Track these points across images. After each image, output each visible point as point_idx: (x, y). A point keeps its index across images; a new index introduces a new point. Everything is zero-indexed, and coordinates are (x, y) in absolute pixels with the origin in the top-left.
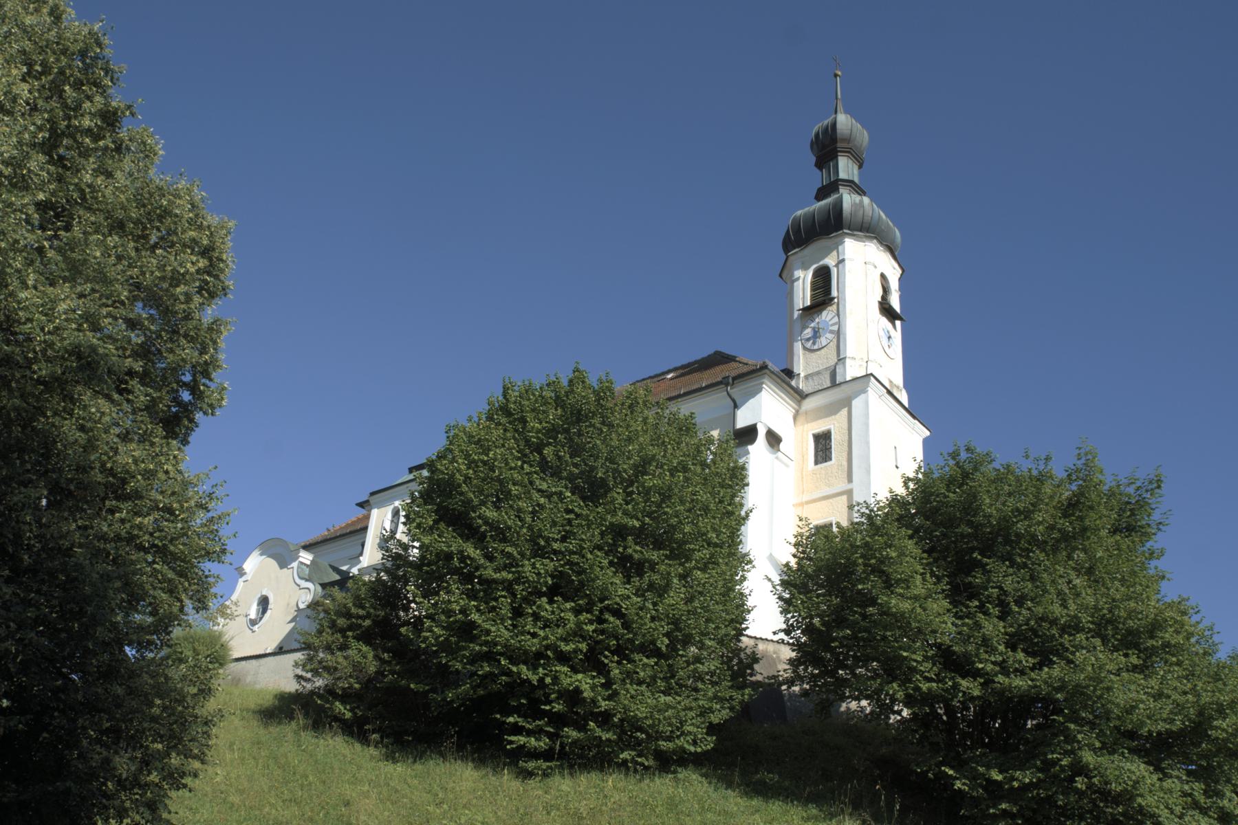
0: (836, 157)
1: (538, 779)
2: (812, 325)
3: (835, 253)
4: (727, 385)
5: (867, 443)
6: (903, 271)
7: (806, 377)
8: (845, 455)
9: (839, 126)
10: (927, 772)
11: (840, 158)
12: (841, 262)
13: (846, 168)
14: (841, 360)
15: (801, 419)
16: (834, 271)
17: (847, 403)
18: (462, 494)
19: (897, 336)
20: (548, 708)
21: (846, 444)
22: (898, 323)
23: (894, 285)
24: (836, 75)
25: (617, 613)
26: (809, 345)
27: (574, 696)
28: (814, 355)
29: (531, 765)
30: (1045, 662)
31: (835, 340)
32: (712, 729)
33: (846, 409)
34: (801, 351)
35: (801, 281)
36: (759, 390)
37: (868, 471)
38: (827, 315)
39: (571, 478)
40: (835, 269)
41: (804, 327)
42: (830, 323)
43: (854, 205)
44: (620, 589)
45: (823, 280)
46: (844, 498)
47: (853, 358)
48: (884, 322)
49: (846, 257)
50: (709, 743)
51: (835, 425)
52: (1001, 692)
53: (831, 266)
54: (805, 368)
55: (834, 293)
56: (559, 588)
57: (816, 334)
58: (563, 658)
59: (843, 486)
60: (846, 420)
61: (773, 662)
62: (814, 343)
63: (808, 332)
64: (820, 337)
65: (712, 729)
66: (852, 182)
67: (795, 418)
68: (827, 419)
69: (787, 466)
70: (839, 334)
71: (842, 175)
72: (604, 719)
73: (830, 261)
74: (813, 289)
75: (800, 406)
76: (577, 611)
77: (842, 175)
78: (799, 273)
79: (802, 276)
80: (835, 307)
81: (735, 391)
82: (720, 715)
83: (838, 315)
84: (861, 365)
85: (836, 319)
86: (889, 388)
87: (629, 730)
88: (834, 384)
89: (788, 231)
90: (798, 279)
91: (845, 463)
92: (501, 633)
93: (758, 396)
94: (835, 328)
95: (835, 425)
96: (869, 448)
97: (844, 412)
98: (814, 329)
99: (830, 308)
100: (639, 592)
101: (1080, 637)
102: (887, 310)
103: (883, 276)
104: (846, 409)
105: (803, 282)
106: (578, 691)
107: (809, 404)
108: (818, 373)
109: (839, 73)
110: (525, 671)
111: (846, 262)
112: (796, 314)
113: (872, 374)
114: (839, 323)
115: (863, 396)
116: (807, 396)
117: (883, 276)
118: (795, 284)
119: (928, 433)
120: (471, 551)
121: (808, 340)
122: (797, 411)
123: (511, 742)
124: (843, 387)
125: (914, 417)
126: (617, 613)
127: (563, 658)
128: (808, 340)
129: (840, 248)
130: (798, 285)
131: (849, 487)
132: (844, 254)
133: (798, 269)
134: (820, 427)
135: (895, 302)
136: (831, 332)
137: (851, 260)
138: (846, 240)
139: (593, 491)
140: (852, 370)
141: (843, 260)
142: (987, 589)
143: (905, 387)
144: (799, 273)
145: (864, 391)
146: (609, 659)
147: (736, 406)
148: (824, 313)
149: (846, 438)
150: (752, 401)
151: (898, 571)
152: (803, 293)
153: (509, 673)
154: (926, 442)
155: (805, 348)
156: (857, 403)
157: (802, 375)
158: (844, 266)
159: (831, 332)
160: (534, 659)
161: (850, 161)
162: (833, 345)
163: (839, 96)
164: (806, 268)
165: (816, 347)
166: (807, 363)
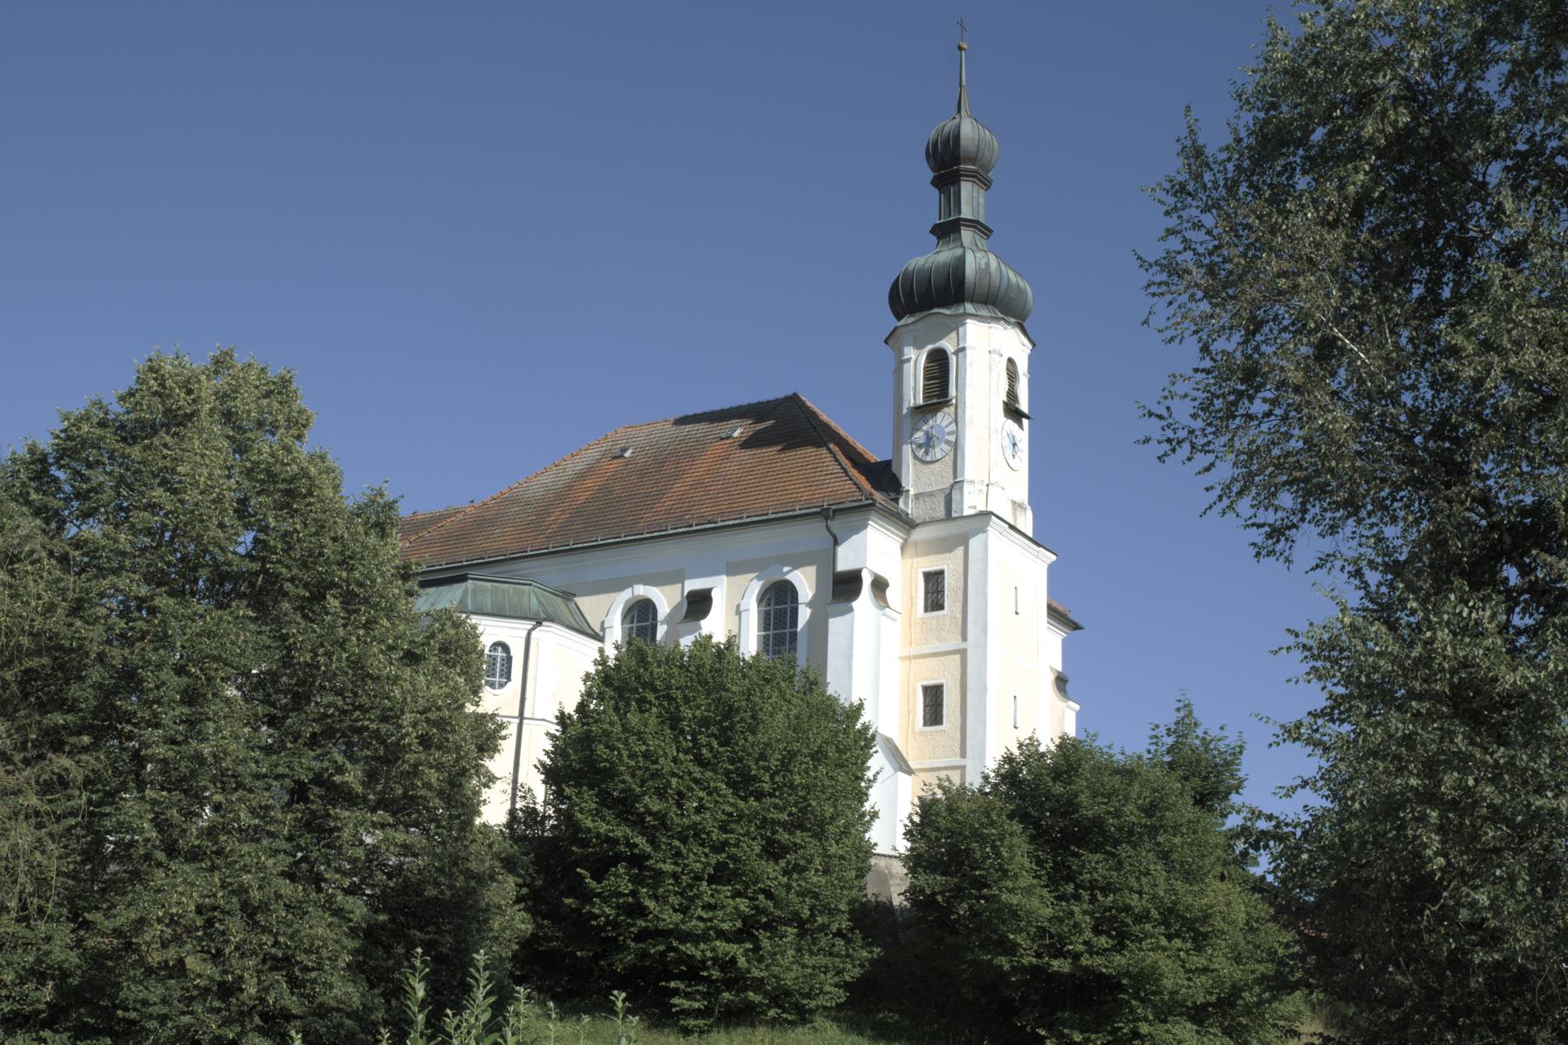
0: (958, 182)
1: (696, 1035)
2: (925, 428)
3: (954, 335)
4: (827, 518)
5: (985, 596)
6: (1034, 345)
7: (917, 496)
8: (959, 605)
9: (963, 141)
10: (1026, 1026)
11: (963, 184)
12: (961, 350)
13: (971, 199)
14: (957, 484)
15: (909, 550)
16: (953, 360)
17: (963, 540)
18: (624, 782)
19: (1022, 435)
20: (705, 974)
21: (961, 593)
22: (1025, 422)
23: (1022, 367)
24: (960, 49)
25: (769, 895)
26: (920, 453)
27: (728, 964)
28: (925, 468)
29: (692, 1022)
30: (1120, 947)
31: (952, 454)
32: (847, 986)
33: (962, 548)
34: (911, 460)
35: (912, 363)
36: (865, 526)
37: (984, 631)
38: (942, 419)
39: (727, 773)
40: (954, 358)
41: (915, 429)
42: (947, 430)
43: (979, 271)
44: (771, 872)
45: (939, 367)
46: (957, 657)
47: (972, 482)
48: (1011, 425)
49: (968, 344)
50: (842, 996)
51: (948, 563)
52: (1086, 969)
53: (949, 353)
54: (915, 484)
55: (952, 391)
56: (719, 876)
57: (929, 443)
58: (721, 934)
59: (956, 643)
60: (961, 561)
61: (884, 878)
62: (927, 453)
63: (919, 436)
64: (934, 447)
65: (847, 986)
66: (977, 222)
67: (903, 548)
68: (940, 556)
69: (894, 620)
70: (956, 447)
71: (966, 212)
72: (758, 985)
73: (948, 345)
74: (926, 379)
75: (909, 536)
76: (736, 894)
77: (966, 212)
78: (910, 352)
79: (914, 357)
80: (952, 409)
81: (836, 525)
82: (852, 973)
83: (956, 421)
84: (980, 491)
85: (953, 427)
86: (1012, 523)
87: (780, 997)
88: (949, 515)
89: (897, 280)
90: (909, 360)
91: (959, 616)
92: (670, 918)
93: (862, 533)
94: (952, 438)
95: (948, 563)
96: (986, 603)
97: (960, 551)
98: (927, 433)
99: (946, 410)
100: (786, 872)
101: (1148, 927)
102: (1012, 412)
103: (1010, 361)
104: (962, 548)
105: (916, 360)
106: (733, 960)
107: (919, 534)
108: (931, 494)
109: (965, 46)
110: (689, 949)
111: (968, 351)
112: (905, 411)
113: (992, 513)
114: (956, 432)
115: (981, 536)
116: (917, 525)
117: (1010, 361)
118: (906, 366)
119: (1054, 558)
120: (640, 840)
121: (920, 446)
122: (905, 540)
123: (675, 1006)
124: (960, 522)
125: (1038, 545)
126: (769, 895)
127: (721, 934)
128: (920, 446)
129: (961, 329)
130: (909, 368)
131: (963, 646)
132: (965, 341)
133: (909, 345)
134: (932, 563)
135: (1024, 406)
136: (948, 442)
137: (974, 348)
138: (969, 321)
139: (743, 783)
140: (971, 502)
141: (964, 349)
142: (1081, 874)
143: (1030, 503)
144: (910, 352)
145: (984, 531)
146: (762, 935)
147: (836, 543)
148: (940, 415)
149: (961, 584)
150: (854, 538)
151: (1012, 868)
152: (914, 390)
153: (675, 950)
154: (1051, 569)
155: (915, 457)
156: (974, 543)
157: (912, 492)
158: (965, 356)
159: (948, 442)
160: (695, 939)
161: (976, 186)
162: (949, 459)
163: (964, 83)
164: (919, 347)
165: (928, 458)
166: (917, 477)
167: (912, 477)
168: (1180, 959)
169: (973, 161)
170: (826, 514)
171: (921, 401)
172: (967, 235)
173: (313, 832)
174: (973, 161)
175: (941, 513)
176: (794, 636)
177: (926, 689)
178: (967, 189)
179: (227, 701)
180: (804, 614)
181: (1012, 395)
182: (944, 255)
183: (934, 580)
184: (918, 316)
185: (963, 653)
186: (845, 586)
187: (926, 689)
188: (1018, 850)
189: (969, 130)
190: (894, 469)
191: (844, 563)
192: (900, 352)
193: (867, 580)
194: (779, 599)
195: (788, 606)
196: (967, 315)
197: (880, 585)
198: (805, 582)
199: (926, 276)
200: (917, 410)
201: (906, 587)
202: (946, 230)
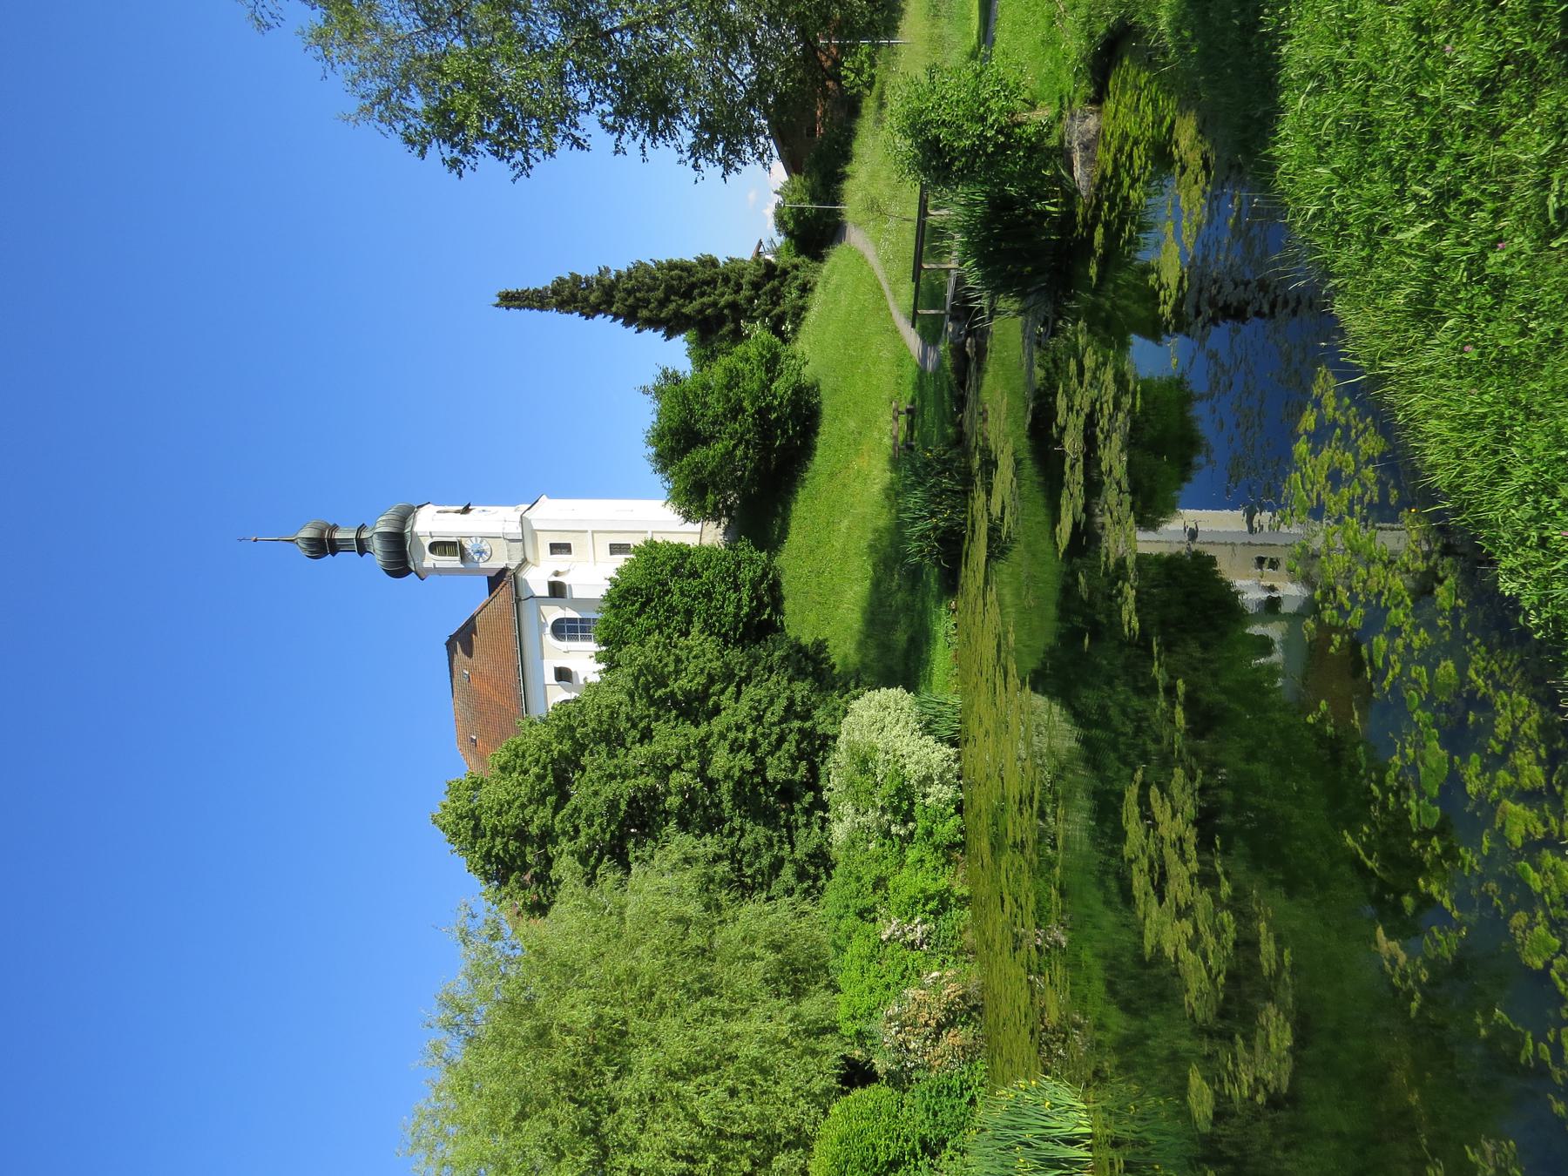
13: (345, 534)
16: (435, 539)
17: (534, 532)
38: (468, 545)
57: (480, 552)
71: (353, 536)
73: (427, 542)
89: (387, 572)
105: (430, 560)
107: (530, 557)
152: (453, 562)
167: (498, 563)
168: (703, 1016)
169: (323, 532)
170: (518, 601)
171: (458, 558)
172: (364, 535)
173: (621, 831)
174: (323, 532)
175: (520, 544)
176: (582, 620)
177: (612, 553)
178: (338, 535)
179: (1336, 728)
180: (571, 614)
181: (457, 512)
182: (376, 545)
183: (557, 548)
184: (410, 558)
185: (593, 532)
186: (557, 590)
187: (612, 553)
188: (698, 455)
189: (307, 533)
190: (493, 575)
191: (544, 591)
192: (429, 570)
193: (554, 579)
194: (562, 629)
195: (566, 625)
196: (411, 531)
197: (557, 574)
198: (553, 613)
199: (388, 554)
200: (463, 559)
201: (560, 561)
202: (362, 547)
